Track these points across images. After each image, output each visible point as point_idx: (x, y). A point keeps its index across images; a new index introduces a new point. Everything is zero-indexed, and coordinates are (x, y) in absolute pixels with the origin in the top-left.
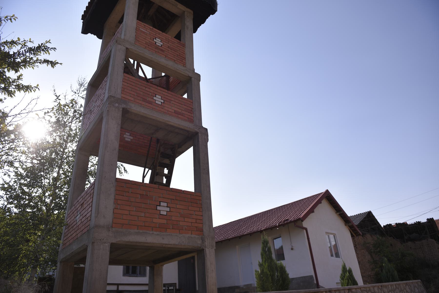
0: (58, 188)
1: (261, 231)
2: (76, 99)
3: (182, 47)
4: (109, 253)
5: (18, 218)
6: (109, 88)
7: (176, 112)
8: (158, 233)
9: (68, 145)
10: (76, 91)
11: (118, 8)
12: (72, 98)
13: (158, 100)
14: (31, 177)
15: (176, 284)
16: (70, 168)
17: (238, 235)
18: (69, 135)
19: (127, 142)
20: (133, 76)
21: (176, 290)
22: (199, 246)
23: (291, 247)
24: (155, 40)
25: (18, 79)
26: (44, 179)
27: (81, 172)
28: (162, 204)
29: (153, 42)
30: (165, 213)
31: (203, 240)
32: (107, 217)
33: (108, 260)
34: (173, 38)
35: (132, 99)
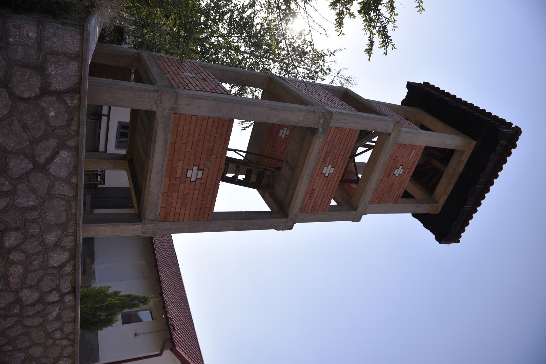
0: (228, 51)
1: (161, 294)
2: (331, 73)
3: (394, 199)
4: (144, 109)
5: (194, 7)
6: (342, 113)
7: (313, 191)
8: (165, 167)
9: (276, 64)
10: (340, 74)
11: (438, 124)
12: (332, 69)
13: (328, 170)
14: (240, 23)
15: (104, 184)
16: (250, 65)
17: (159, 264)
18: (288, 65)
19: (278, 132)
20: (357, 140)
21: (97, 184)
22: (146, 216)
23: (138, 333)
24: (401, 167)
25: (350, 13)
26: (238, 37)
27: (243, 80)
28: (200, 172)
29: (399, 164)
30: (189, 175)
31: (153, 221)
32: (187, 108)
33: (136, 108)
34: (404, 189)
35: (329, 140)
